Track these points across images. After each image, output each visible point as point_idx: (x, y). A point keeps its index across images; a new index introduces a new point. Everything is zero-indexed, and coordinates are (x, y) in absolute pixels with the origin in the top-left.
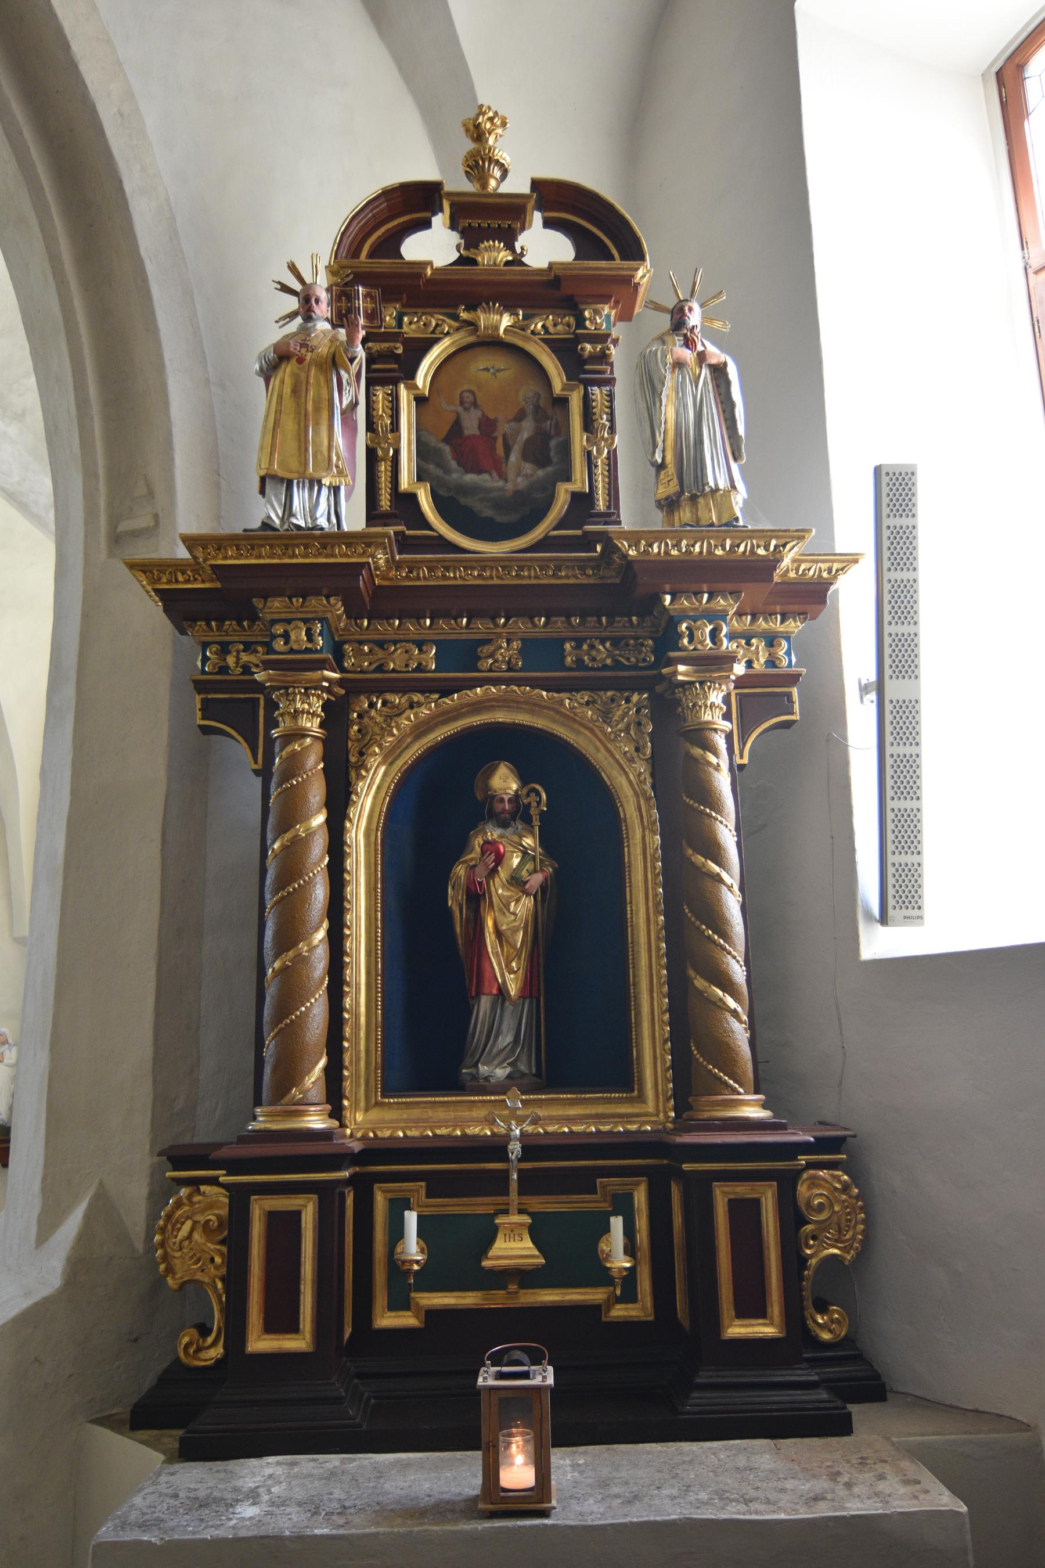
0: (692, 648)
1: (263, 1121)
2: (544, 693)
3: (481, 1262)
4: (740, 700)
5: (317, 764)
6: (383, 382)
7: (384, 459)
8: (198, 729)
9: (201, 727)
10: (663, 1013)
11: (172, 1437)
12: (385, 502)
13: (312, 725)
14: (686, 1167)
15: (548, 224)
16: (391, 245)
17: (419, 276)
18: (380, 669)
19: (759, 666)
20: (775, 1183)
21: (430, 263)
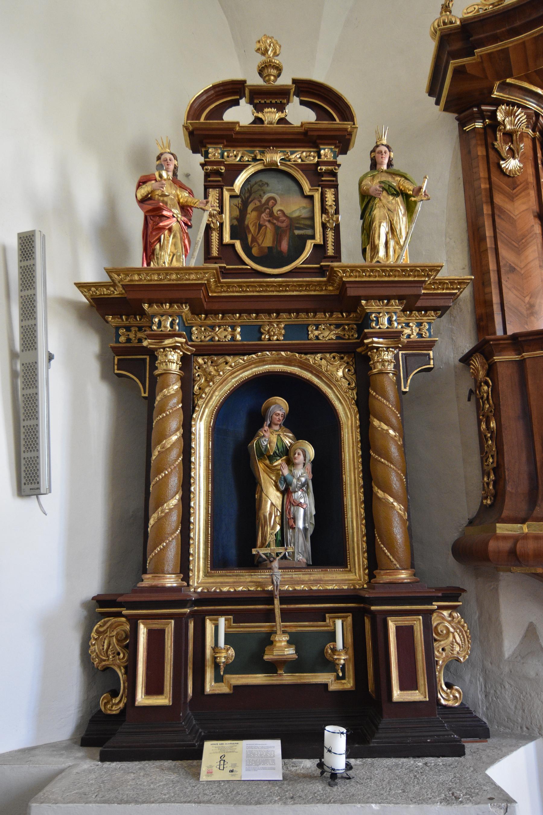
0: (378, 327)
1: (148, 581)
2: (297, 355)
3: (263, 656)
4: (406, 358)
5: (178, 404)
6: (214, 187)
7: (214, 229)
8: (111, 349)
9: (118, 375)
10: (363, 537)
11: (96, 751)
12: (215, 252)
13: (174, 367)
14: (373, 608)
15: (302, 103)
16: (219, 112)
17: (232, 129)
18: (212, 339)
19: (414, 337)
20: (421, 617)
21: (238, 123)
